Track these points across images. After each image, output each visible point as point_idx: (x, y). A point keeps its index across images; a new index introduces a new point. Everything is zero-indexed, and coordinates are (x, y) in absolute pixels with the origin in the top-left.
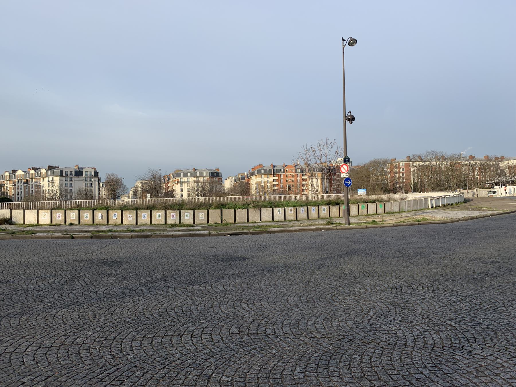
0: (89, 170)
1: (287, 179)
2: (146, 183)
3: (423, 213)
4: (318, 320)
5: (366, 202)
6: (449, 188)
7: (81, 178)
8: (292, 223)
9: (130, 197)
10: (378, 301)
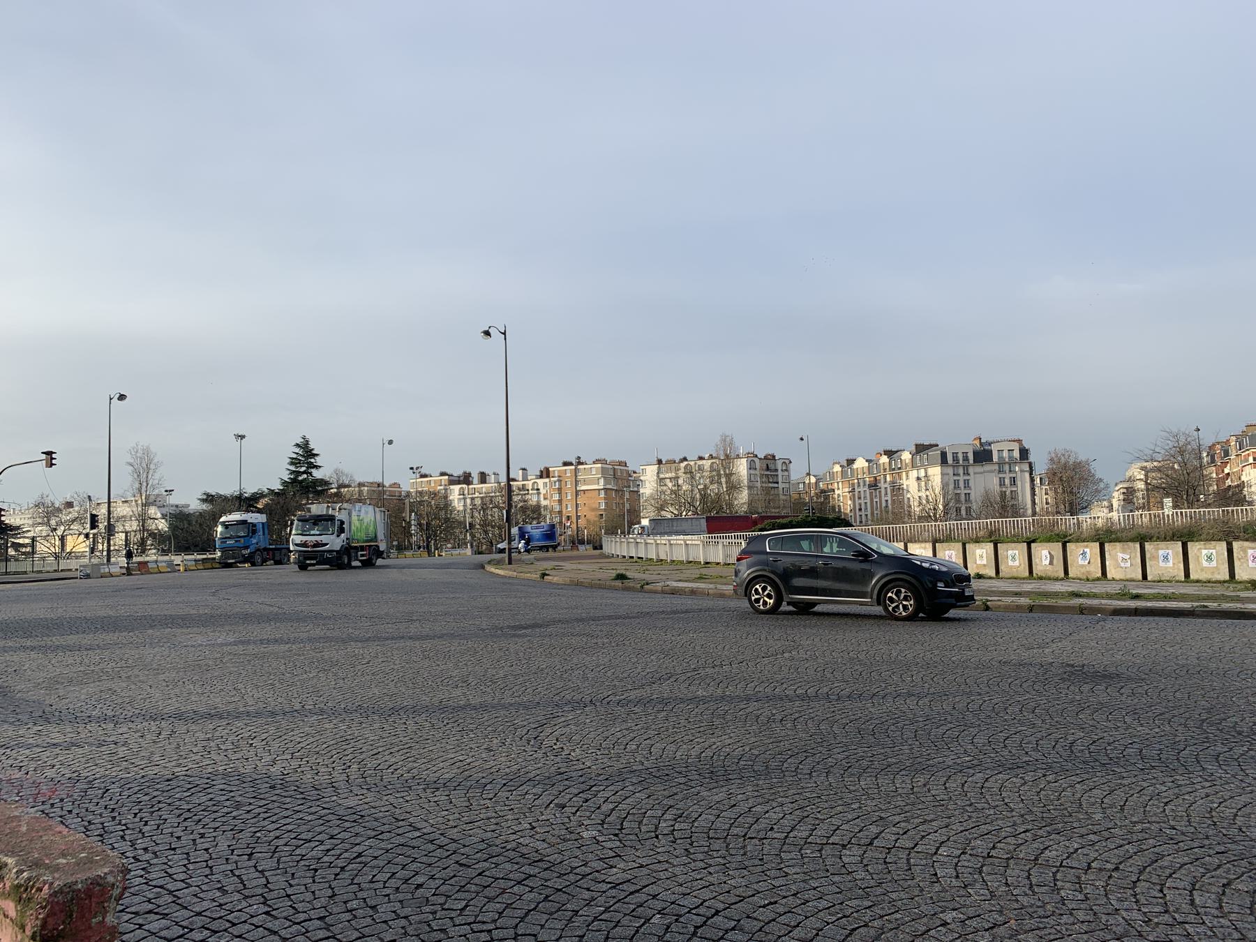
0: (1005, 447)
2: (1158, 470)
7: (988, 467)
9: (1115, 504)
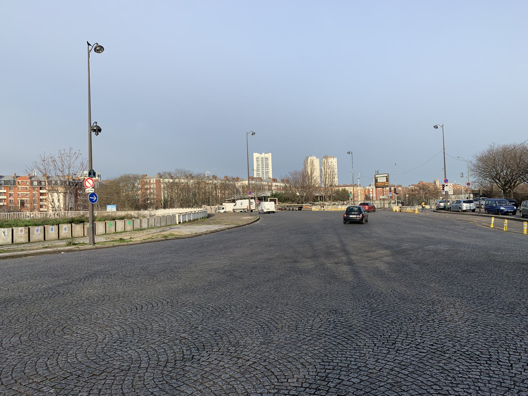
1: (20, 193)
3: (171, 228)
4: (41, 360)
5: (114, 219)
6: (196, 204)
8: (22, 247)
10: (116, 326)
